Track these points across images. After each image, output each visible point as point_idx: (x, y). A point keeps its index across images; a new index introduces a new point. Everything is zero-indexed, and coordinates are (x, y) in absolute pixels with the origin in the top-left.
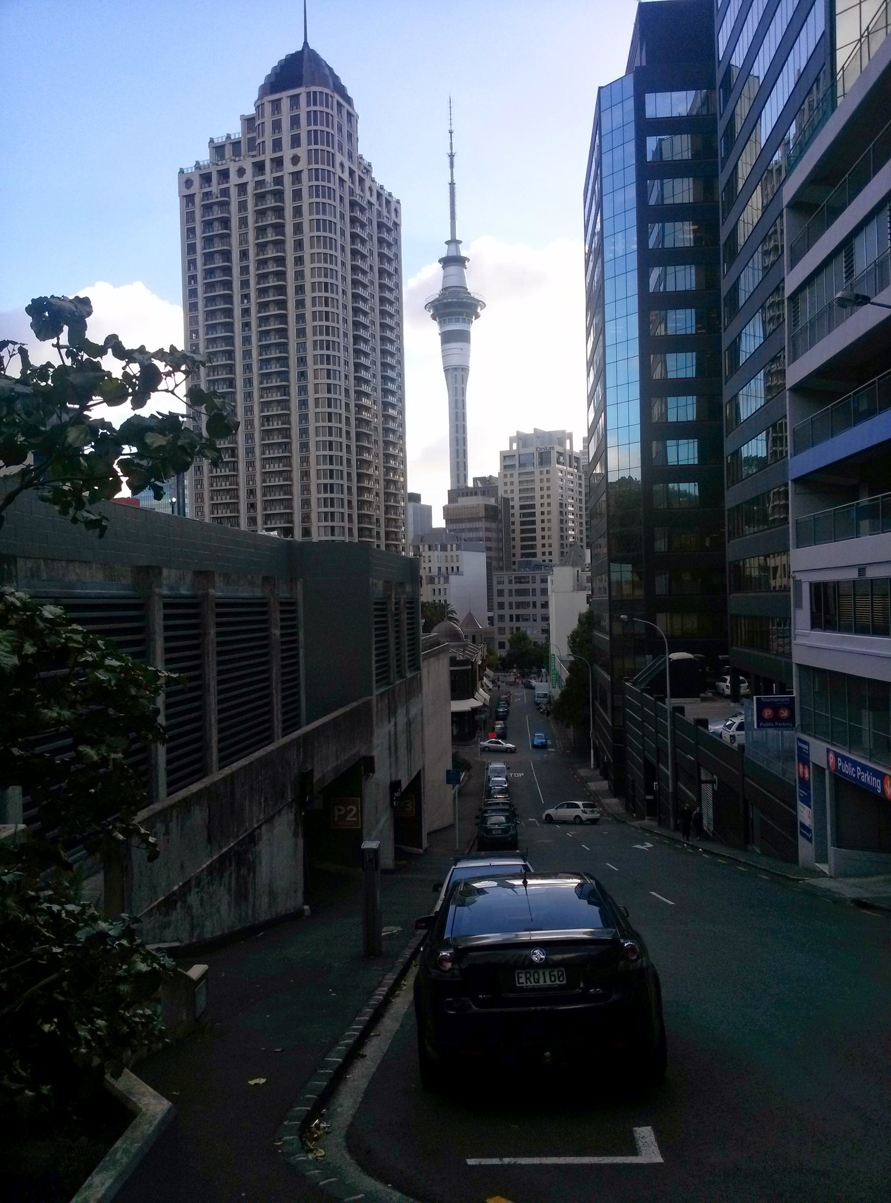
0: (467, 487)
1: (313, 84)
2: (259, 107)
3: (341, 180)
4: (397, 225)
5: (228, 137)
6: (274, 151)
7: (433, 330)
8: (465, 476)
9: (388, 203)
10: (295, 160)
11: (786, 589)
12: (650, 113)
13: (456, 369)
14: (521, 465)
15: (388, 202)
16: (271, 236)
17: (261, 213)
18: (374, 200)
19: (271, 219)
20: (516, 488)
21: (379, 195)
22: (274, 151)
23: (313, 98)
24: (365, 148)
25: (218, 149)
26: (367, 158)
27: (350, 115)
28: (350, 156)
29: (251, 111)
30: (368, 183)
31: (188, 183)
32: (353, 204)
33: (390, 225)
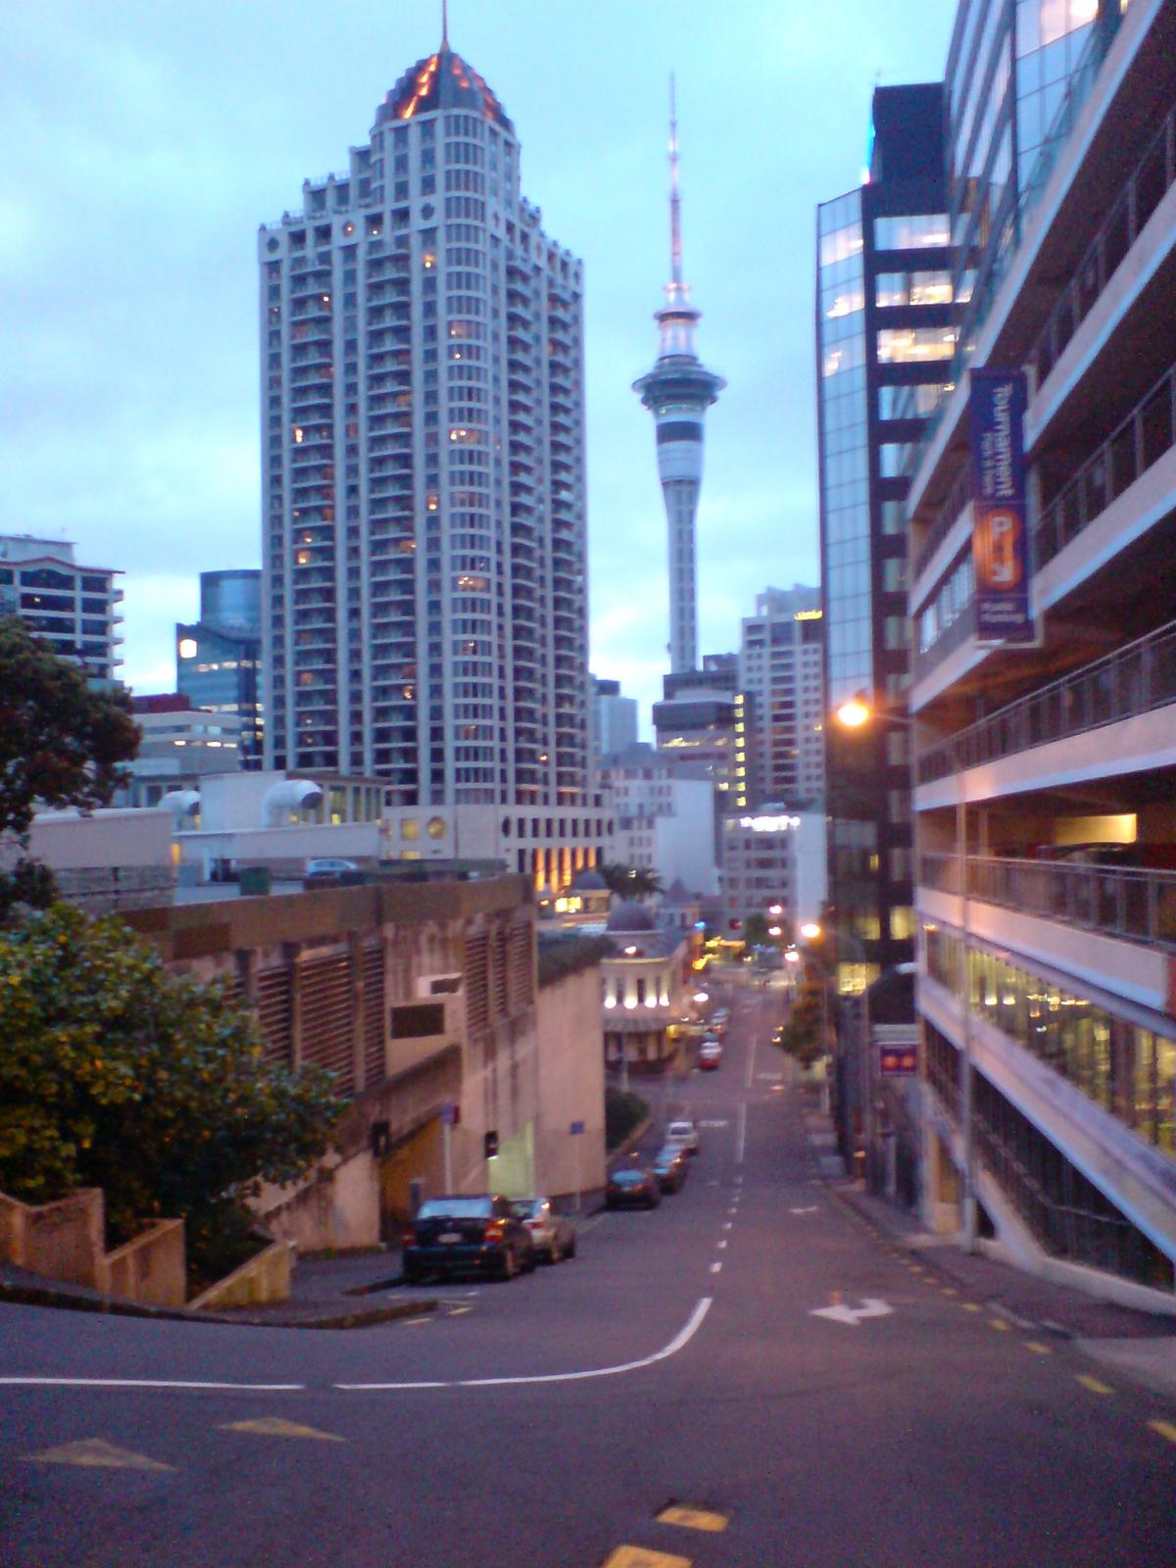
0: (694, 671)
1: (455, 105)
2: (378, 136)
3: (495, 240)
4: (577, 296)
5: (331, 177)
6: (397, 200)
7: (645, 422)
8: (693, 650)
9: (565, 265)
10: (427, 211)
11: (1146, 933)
12: (884, 355)
13: (679, 482)
14: (776, 641)
15: (564, 265)
16: (390, 321)
17: (376, 288)
18: (543, 263)
19: (391, 297)
20: (767, 675)
21: (551, 256)
22: (397, 200)
23: (456, 125)
24: (534, 187)
25: (315, 196)
26: (534, 201)
27: (508, 145)
28: (509, 203)
29: (364, 141)
30: (534, 240)
31: (273, 245)
32: (512, 272)
33: (567, 296)
